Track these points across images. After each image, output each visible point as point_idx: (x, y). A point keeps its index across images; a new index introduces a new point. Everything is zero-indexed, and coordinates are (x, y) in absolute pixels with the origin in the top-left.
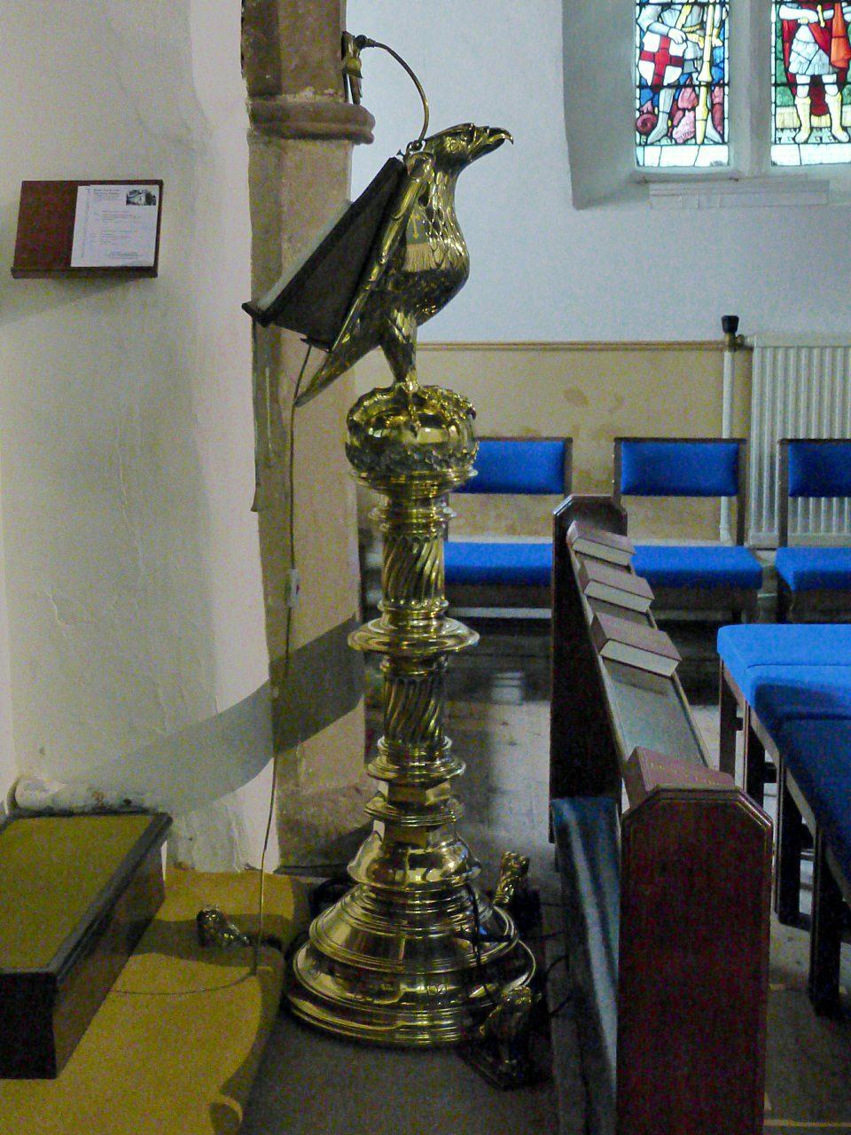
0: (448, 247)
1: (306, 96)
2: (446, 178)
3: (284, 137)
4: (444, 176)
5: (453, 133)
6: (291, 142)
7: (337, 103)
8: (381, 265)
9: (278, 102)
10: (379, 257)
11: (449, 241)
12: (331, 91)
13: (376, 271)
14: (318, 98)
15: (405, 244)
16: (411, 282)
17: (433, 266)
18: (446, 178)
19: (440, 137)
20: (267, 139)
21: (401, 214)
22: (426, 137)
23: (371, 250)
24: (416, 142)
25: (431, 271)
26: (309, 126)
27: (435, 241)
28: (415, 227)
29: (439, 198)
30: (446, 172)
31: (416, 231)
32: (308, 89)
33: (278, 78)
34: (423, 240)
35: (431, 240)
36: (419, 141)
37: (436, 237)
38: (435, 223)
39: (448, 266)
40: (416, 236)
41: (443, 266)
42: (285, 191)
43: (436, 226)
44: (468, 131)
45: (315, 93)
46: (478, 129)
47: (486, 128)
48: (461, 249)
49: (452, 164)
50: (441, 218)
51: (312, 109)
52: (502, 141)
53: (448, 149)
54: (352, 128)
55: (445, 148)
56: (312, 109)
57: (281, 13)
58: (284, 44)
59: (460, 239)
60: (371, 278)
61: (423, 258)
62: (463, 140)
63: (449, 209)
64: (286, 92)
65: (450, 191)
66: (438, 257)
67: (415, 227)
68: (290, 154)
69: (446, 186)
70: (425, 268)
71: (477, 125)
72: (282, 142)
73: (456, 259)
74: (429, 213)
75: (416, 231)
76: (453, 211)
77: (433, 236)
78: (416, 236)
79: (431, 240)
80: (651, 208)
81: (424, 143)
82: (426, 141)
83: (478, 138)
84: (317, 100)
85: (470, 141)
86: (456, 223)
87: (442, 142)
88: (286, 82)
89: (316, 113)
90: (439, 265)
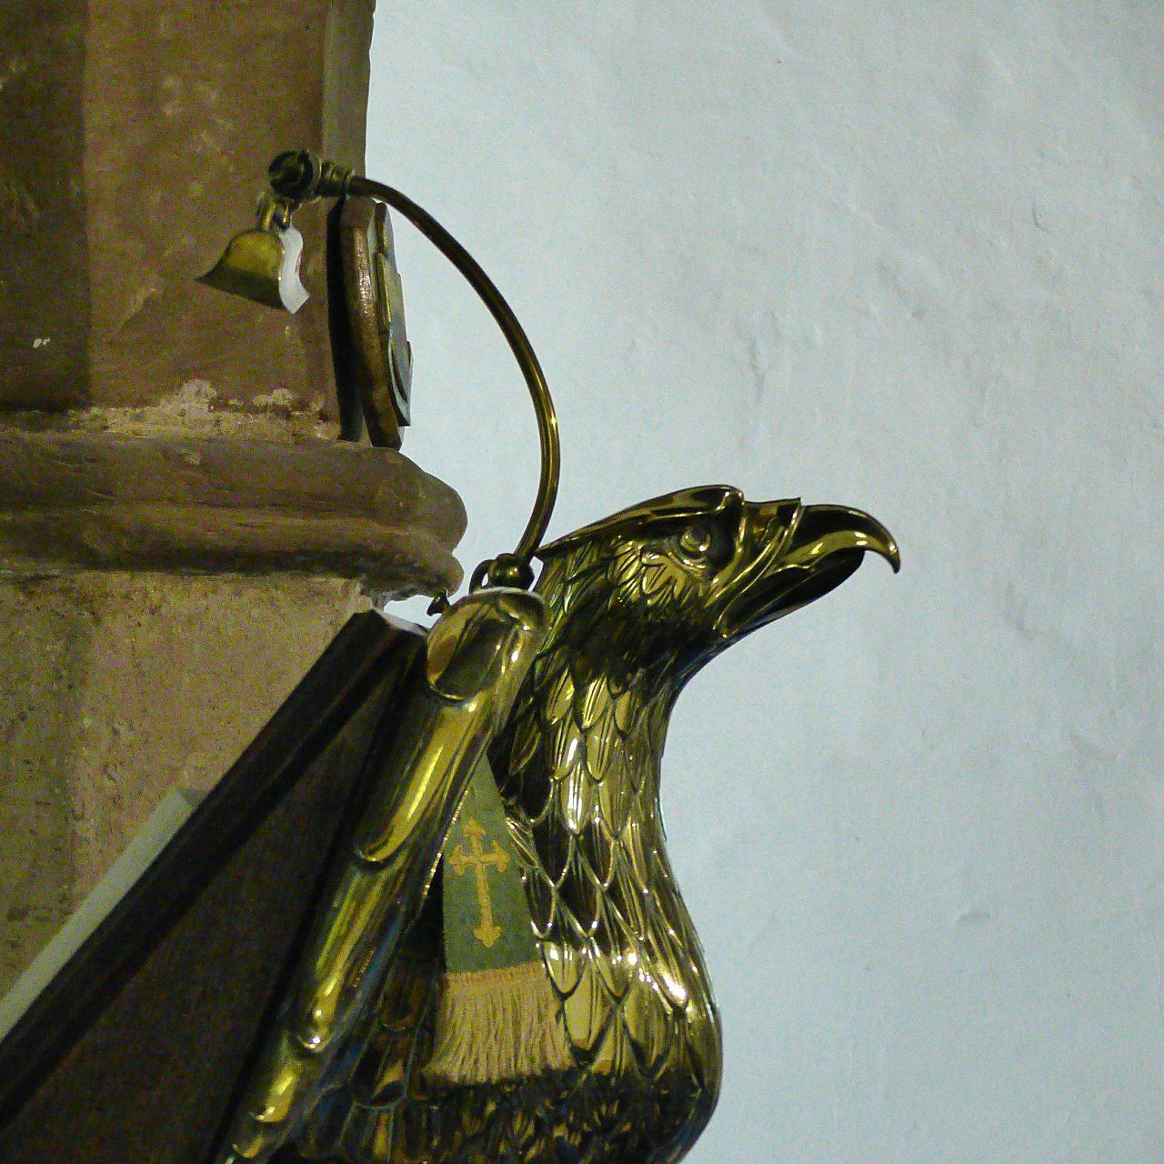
0: (623, 983)
1: (186, 413)
2: (624, 701)
3: (92, 561)
4: (614, 697)
5: (653, 523)
6: (117, 580)
7: (301, 440)
8: (305, 1054)
9: (76, 435)
10: (303, 1023)
11: (632, 958)
12: (281, 396)
13: (284, 1084)
14: (231, 422)
15: (443, 967)
16: (470, 1126)
17: (560, 1058)
18: (624, 701)
19: (603, 538)
20: (29, 568)
21: (395, 841)
22: (549, 538)
23: (280, 992)
24: (504, 561)
25: (549, 1081)
26: (179, 521)
27: (569, 955)
28: (485, 900)
29: (592, 781)
30: (619, 680)
31: (487, 914)
32: (190, 388)
33: (78, 352)
34: (519, 952)
35: (553, 953)
36: (519, 559)
37: (576, 943)
38: (596, 886)
39: (626, 1058)
40: (488, 934)
41: (604, 1058)
42: (87, 761)
43: (577, 897)
44: (711, 515)
45: (219, 404)
46: (754, 509)
47: (786, 508)
48: (678, 991)
49: (656, 651)
50: (599, 866)
51: (195, 459)
52: (846, 562)
53: (632, 587)
54: (365, 531)
55: (613, 586)
56: (195, 459)
57: (98, 116)
58: (102, 226)
59: (687, 955)
60: (262, 1110)
61: (517, 1023)
62: (694, 555)
63: (631, 829)
64: (108, 402)
65: (642, 750)
66: (581, 1019)
67: (485, 900)
68: (116, 624)
69: (622, 734)
70: (524, 1067)
71: (751, 495)
72: (86, 579)
73: (657, 1029)
74: (550, 840)
75: (487, 914)
76: (652, 836)
77: (562, 935)
78: (488, 934)
79: (553, 953)
80: (37, 803)
81: (536, 565)
82: (547, 555)
83: (753, 548)
84: (224, 426)
85: (718, 562)
86: (666, 888)
87: (610, 559)
88: (102, 363)
89: (214, 474)
90: (583, 1055)
